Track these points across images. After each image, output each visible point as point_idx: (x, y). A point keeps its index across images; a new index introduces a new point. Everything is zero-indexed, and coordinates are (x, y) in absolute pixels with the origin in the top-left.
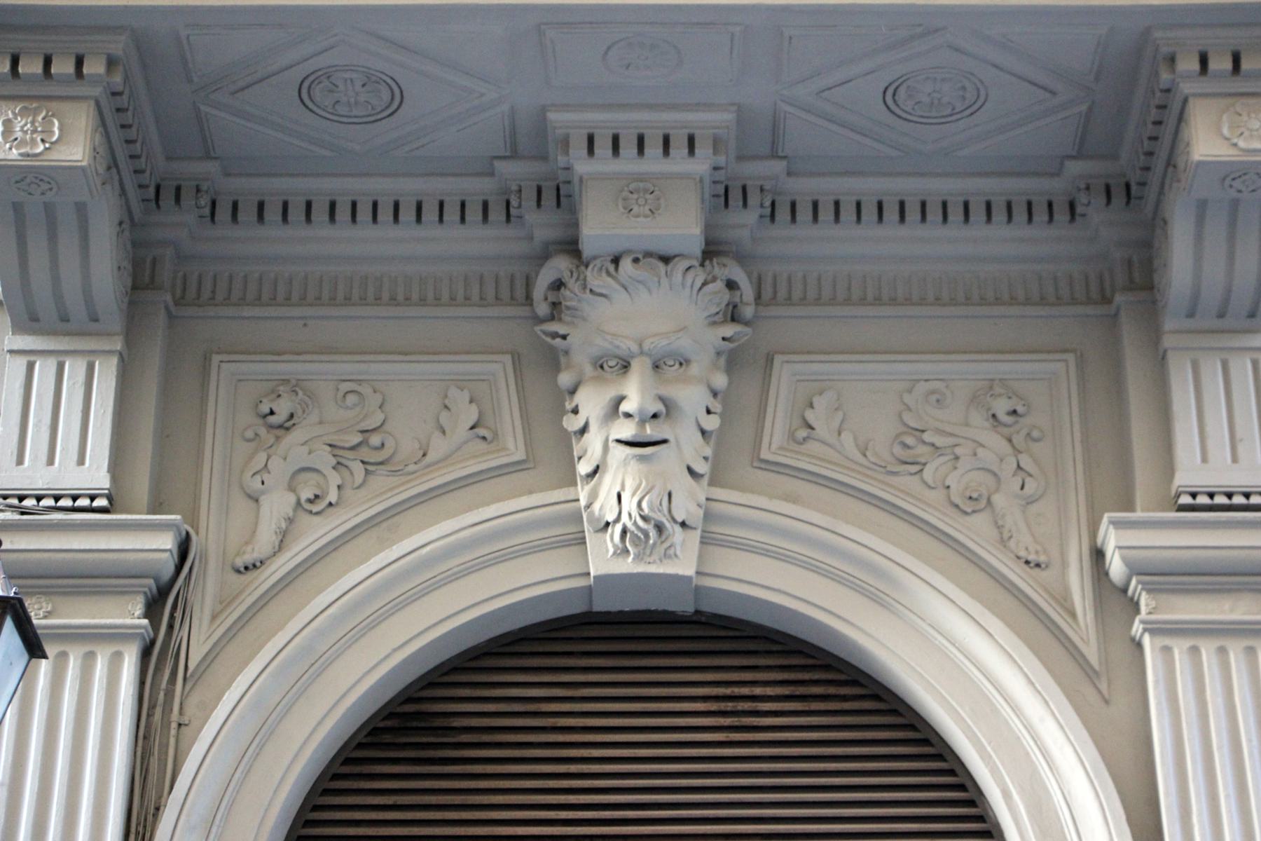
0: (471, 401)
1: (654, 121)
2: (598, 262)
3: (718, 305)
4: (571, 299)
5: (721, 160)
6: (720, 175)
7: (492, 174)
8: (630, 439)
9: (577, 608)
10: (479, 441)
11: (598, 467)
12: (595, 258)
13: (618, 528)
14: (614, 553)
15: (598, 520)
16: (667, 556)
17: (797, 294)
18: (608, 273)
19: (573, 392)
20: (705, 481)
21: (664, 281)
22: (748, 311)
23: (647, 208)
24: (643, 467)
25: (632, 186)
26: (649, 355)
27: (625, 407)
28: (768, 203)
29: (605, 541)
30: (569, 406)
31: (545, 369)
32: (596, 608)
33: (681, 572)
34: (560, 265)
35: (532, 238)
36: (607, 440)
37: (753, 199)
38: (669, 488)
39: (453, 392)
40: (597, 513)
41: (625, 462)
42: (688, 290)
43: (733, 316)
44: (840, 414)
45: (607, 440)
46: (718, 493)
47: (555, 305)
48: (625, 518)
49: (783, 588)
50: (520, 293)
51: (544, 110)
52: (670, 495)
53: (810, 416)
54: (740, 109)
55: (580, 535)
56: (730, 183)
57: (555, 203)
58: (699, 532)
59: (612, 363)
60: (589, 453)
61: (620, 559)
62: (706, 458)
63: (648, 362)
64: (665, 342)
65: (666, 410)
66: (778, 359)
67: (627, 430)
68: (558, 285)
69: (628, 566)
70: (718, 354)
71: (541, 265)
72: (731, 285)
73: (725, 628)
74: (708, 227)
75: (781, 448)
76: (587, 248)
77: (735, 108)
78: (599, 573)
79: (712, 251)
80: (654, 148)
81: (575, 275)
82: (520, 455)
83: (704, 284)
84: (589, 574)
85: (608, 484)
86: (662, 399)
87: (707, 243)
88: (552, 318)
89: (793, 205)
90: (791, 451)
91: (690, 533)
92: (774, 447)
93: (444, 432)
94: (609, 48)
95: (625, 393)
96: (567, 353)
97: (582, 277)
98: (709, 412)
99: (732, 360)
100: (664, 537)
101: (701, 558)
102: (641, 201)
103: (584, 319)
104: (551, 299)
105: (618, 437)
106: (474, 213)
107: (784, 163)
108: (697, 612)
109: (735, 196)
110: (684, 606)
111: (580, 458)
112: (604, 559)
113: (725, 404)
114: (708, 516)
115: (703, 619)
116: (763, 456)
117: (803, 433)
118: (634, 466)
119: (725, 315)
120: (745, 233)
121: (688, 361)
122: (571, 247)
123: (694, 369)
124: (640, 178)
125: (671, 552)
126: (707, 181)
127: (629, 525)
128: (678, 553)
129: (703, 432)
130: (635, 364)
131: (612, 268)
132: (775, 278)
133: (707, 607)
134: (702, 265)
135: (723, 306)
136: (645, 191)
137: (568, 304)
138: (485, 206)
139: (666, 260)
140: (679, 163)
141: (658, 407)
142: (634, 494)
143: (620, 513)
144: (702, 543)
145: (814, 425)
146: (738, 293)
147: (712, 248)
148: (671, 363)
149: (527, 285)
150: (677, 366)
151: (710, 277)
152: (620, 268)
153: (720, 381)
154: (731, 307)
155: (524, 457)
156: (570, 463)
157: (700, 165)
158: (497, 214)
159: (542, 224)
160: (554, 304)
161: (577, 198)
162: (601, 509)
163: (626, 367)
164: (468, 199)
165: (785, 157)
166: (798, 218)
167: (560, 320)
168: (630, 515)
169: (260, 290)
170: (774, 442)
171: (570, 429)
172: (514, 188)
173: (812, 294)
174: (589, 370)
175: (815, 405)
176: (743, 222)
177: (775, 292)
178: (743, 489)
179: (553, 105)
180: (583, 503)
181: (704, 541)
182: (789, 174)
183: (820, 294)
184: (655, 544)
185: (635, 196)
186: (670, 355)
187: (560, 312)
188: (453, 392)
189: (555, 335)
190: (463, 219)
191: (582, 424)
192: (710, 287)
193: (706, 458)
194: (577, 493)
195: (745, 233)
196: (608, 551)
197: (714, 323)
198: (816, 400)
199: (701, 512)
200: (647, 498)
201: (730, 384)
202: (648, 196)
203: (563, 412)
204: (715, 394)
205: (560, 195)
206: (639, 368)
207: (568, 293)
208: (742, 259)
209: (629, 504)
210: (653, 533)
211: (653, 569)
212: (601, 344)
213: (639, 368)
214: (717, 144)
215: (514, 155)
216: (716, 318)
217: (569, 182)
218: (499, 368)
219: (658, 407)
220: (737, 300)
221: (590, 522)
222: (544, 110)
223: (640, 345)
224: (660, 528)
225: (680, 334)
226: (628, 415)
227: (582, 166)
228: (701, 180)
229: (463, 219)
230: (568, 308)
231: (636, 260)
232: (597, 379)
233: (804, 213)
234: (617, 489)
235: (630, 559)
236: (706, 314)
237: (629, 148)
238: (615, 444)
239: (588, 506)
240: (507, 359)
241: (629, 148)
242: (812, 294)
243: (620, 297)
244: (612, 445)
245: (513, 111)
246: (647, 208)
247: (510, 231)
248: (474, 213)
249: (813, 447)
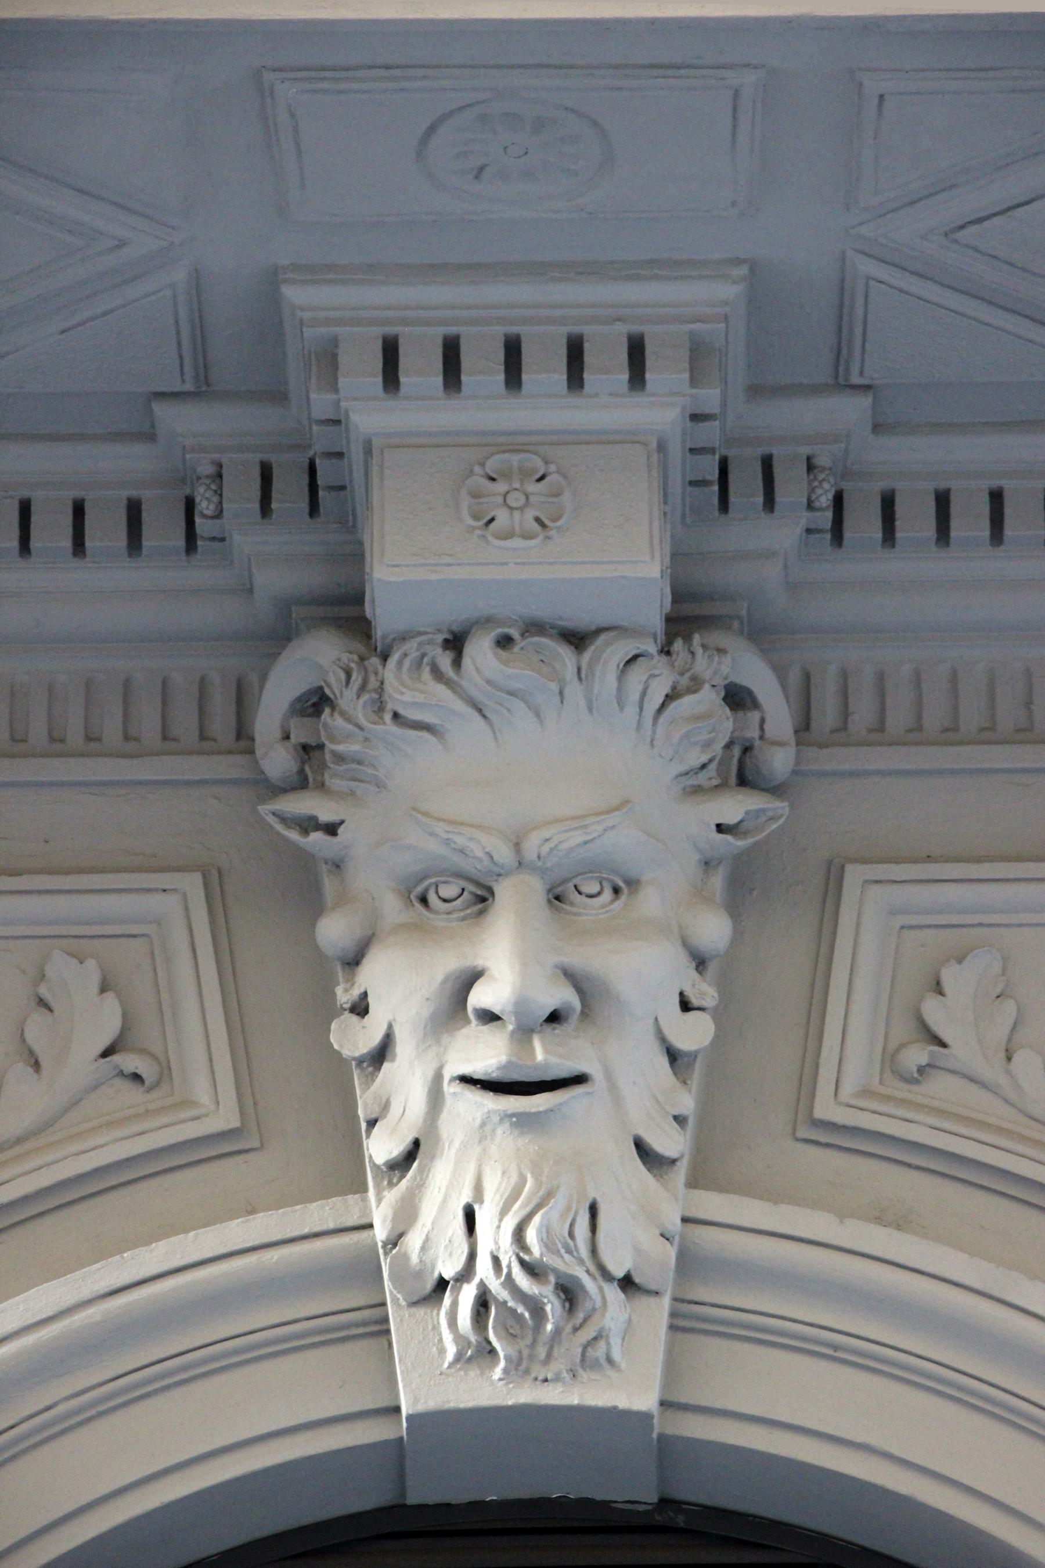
0: (103, 989)
1: (544, 307)
2: (411, 646)
3: (707, 745)
4: (348, 737)
5: (710, 397)
6: (710, 434)
7: (151, 437)
8: (495, 1075)
9: (367, 1496)
10: (119, 1082)
11: (416, 1143)
12: (404, 637)
13: (468, 1293)
14: (459, 1357)
15: (419, 1275)
16: (590, 1361)
17: (898, 719)
18: (437, 673)
19: (353, 961)
20: (680, 1174)
21: (575, 691)
22: (779, 761)
23: (530, 514)
24: (528, 1144)
25: (492, 465)
26: (542, 872)
27: (480, 997)
28: (825, 499)
29: (436, 1328)
30: (344, 996)
31: (285, 902)
32: (413, 1498)
33: (623, 1403)
34: (319, 656)
35: (251, 591)
36: (438, 1077)
37: (791, 488)
38: (592, 1194)
39: (60, 965)
40: (414, 1259)
41: (483, 1131)
42: (631, 710)
43: (743, 772)
44: (1010, 1008)
45: (438, 1077)
46: (712, 1204)
47: (309, 750)
48: (484, 1268)
49: (873, 1441)
50: (222, 725)
51: (272, 280)
52: (593, 1210)
53: (934, 1011)
54: (757, 275)
55: (375, 1313)
56: (731, 453)
57: (304, 505)
58: (666, 1301)
59: (447, 891)
60: (395, 1110)
61: (473, 1372)
62: (680, 1120)
63: (536, 887)
64: (577, 838)
65: (580, 1004)
66: (854, 875)
67: (486, 1053)
68: (316, 703)
69: (492, 1389)
70: (707, 864)
71: (274, 656)
72: (737, 698)
73: (726, 1541)
74: (679, 558)
75: (866, 1092)
76: (385, 614)
77: (743, 270)
78: (421, 1408)
79: (687, 618)
80: (545, 372)
81: (357, 678)
82: (226, 1118)
83: (669, 698)
84: (397, 1410)
85: (443, 1187)
86: (571, 976)
87: (678, 597)
88: (301, 783)
89: (888, 503)
90: (889, 1099)
91: (644, 1303)
92: (848, 1089)
93: (36, 1065)
94: (432, 129)
95: (479, 963)
96: (337, 866)
97: (373, 683)
98: (686, 1006)
99: (743, 878)
100: (580, 1316)
101: (673, 1369)
102: (516, 499)
103: (380, 785)
104: (298, 736)
105: (467, 1070)
106: (106, 531)
107: (866, 401)
108: (665, 1503)
109: (746, 486)
110: (635, 1488)
111: (372, 1123)
112: (433, 1371)
113: (723, 985)
114: (688, 1263)
115: (681, 1521)
116: (819, 1113)
117: (917, 1055)
118: (505, 1142)
119: (723, 774)
120: (772, 573)
121: (633, 884)
122: (346, 611)
123: (650, 903)
124: (516, 442)
125: (599, 1351)
126: (676, 451)
127: (495, 1286)
128: (616, 1354)
129: (673, 1056)
130: (505, 892)
131: (445, 661)
132: (844, 675)
133: (695, 1491)
134: (666, 651)
135: (718, 747)
136: (525, 473)
137: (340, 748)
138: (134, 511)
139: (577, 639)
140: (608, 405)
141: (563, 996)
142: (503, 1212)
143: (472, 1257)
144: (672, 1328)
145: (945, 1035)
146: (755, 716)
147: (688, 609)
148: (595, 889)
149: (240, 702)
150: (607, 895)
151: (685, 681)
152: (467, 661)
153: (713, 929)
154: (737, 751)
155: (235, 1123)
156: (349, 1132)
157: (660, 410)
158: (162, 530)
159: (274, 558)
160: (306, 748)
161: (359, 491)
162: (423, 1249)
163: (483, 898)
164: (90, 497)
165: (868, 388)
166: (1008, 532)
167: (321, 786)
168: (496, 1261)
169: (992, 706)
170: (849, 1076)
171: (346, 1053)
172: (208, 469)
173: (934, 718)
174: (393, 909)
175: (947, 988)
176: (766, 547)
177: (845, 714)
178: (775, 1196)
179: (295, 267)
180: (380, 1233)
181: (680, 1325)
182: (877, 428)
183: (919, 717)
184: (557, 1332)
185: (501, 487)
186: (592, 868)
187: (323, 766)
188: (60, 965)
189: (308, 824)
190: (79, 545)
191: (376, 1039)
192: (686, 704)
193: (680, 1120)
194: (366, 1210)
195: (772, 573)
196: (442, 1351)
197: (697, 790)
198: (949, 976)
199: (671, 1253)
200: (537, 1219)
201: (738, 934)
202: (532, 487)
203: (330, 1011)
204: (701, 963)
205: (317, 486)
206: (516, 902)
207: (339, 722)
208: (761, 634)
209: (494, 1234)
210: (553, 1307)
211: (553, 1396)
212: (424, 845)
213: (516, 902)
214: (699, 357)
215: (202, 389)
216: (702, 779)
217: (340, 455)
218: (175, 906)
219: (563, 996)
220: (753, 733)
221: (394, 1277)
222: (272, 280)
223: (517, 847)
224: (569, 1293)
225: (615, 818)
226: (489, 1017)
227: (371, 416)
228: (662, 447)
229: (79, 545)
230: (340, 758)
231: (504, 642)
232: (418, 930)
233: (916, 521)
234: (463, 1194)
235: (498, 1372)
236: (678, 768)
237: (482, 370)
238: (457, 1087)
239: (394, 1241)
240: (192, 884)
241: (482, 370)
242: (934, 718)
243: (467, 730)
244: (451, 1089)
245: (197, 280)
246: (530, 514)
247: (198, 574)
248: (106, 531)
249: (941, 1088)
